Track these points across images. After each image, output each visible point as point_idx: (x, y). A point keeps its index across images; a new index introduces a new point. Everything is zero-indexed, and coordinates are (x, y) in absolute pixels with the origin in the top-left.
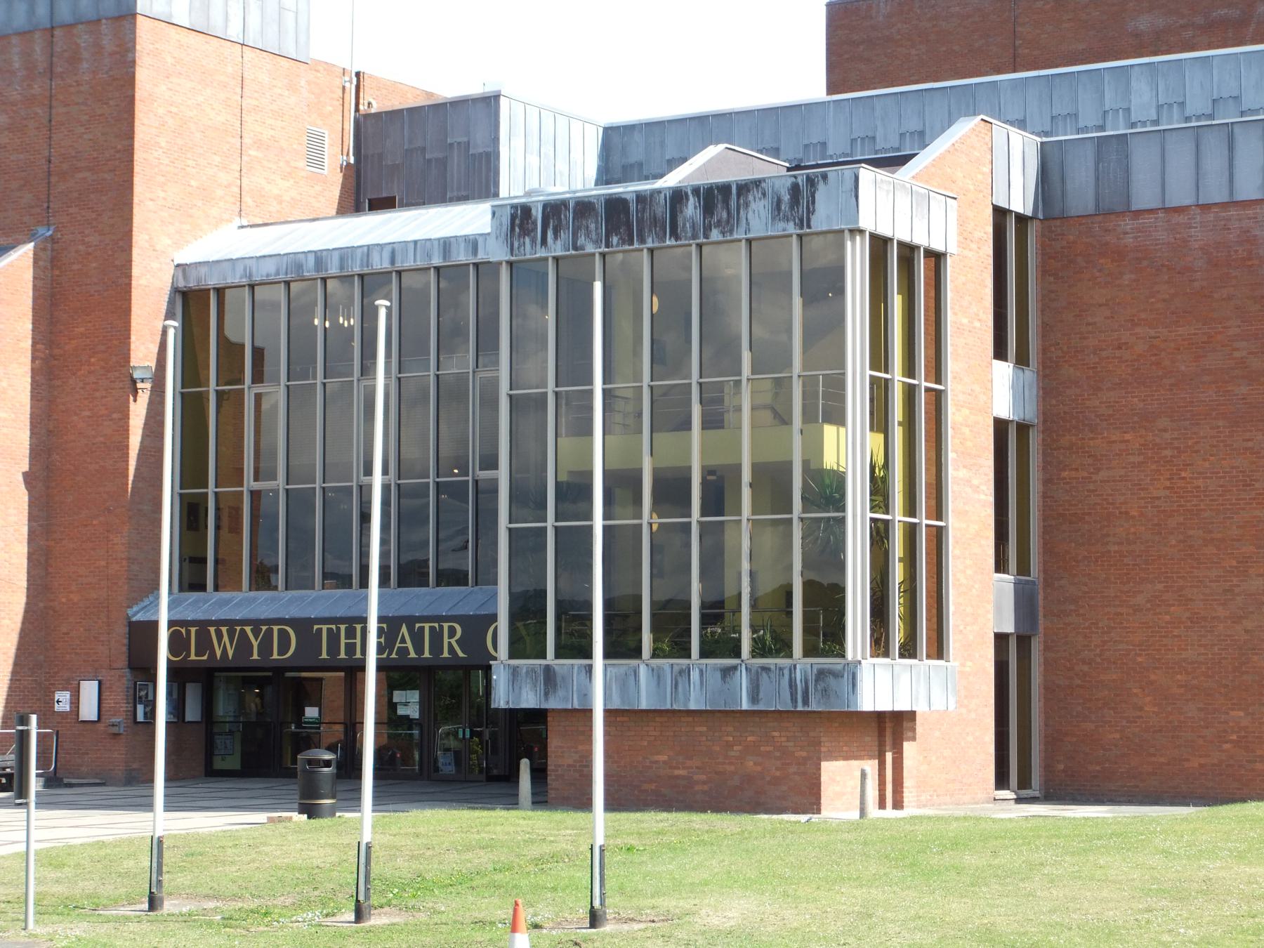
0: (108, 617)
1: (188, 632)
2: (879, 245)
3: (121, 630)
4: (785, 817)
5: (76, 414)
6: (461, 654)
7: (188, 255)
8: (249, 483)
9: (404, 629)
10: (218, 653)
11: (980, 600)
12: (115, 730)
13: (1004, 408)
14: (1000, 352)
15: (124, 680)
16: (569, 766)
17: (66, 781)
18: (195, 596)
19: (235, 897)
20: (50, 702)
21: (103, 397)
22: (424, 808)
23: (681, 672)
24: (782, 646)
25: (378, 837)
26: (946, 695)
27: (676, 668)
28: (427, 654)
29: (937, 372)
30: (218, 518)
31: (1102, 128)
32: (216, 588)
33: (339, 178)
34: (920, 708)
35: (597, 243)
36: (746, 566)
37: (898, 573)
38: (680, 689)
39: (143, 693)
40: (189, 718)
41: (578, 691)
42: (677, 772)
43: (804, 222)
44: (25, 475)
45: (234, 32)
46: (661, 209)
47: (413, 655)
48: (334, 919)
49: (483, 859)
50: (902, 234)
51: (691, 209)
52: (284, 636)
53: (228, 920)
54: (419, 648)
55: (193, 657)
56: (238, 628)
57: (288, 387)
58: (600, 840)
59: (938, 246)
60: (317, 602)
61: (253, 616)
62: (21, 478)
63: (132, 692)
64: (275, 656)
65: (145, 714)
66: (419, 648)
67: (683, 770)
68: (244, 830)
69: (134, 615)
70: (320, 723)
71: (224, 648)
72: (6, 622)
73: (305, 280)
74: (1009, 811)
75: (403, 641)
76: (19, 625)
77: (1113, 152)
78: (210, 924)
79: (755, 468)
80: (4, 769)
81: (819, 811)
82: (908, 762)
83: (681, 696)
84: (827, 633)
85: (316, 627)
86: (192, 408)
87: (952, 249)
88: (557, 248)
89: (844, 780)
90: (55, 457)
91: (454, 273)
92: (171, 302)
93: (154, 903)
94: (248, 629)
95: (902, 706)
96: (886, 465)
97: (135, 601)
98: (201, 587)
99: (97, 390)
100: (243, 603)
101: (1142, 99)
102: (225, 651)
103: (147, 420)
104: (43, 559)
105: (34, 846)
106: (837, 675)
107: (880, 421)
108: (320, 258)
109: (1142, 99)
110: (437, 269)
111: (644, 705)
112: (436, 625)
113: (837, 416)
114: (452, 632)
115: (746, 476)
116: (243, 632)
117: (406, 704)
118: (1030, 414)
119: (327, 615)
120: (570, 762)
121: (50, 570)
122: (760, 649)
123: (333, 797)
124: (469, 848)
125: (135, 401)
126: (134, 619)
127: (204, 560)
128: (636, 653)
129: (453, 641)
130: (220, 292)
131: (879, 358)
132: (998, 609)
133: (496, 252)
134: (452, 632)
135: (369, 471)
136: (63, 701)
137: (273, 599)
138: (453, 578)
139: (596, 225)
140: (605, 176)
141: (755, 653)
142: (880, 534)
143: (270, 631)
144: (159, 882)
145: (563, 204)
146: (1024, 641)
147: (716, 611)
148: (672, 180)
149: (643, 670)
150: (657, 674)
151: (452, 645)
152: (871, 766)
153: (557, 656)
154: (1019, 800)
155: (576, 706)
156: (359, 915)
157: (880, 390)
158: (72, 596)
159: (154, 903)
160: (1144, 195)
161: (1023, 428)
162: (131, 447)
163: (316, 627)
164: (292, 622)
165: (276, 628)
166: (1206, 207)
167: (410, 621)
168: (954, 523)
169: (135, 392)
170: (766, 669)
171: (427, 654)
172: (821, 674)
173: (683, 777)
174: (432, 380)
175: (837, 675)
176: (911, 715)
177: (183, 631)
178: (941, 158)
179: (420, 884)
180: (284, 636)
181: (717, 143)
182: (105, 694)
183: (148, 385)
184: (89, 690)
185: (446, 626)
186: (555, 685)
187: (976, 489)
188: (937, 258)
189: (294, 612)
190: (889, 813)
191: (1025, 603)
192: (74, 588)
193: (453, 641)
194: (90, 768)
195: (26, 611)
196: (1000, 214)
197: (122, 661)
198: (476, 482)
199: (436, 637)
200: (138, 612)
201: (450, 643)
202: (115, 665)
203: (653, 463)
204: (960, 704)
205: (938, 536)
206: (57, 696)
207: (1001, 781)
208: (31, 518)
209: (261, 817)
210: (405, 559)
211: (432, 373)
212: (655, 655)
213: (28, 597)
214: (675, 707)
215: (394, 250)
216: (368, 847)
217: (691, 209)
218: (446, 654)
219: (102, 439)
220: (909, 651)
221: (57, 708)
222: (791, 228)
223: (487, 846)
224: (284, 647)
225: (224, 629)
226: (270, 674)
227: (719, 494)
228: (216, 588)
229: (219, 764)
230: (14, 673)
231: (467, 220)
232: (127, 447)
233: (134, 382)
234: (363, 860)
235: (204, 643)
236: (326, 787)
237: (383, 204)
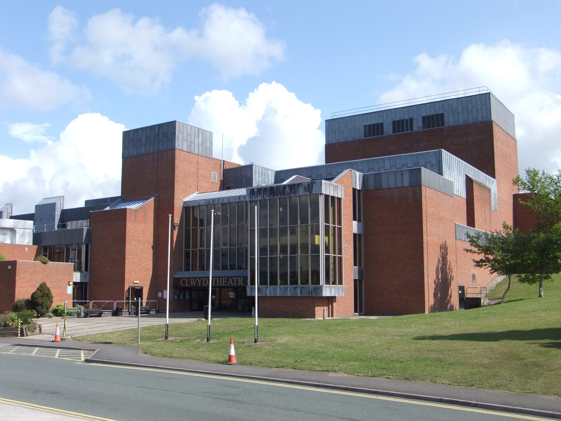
2: (327, 197)
4: (308, 319)
7: (187, 199)
8: (199, 248)
11: (350, 271)
13: (355, 230)
14: (354, 219)
19: (184, 337)
20: (157, 295)
24: (307, 282)
26: (342, 292)
29: (340, 223)
30: (192, 255)
31: (379, 171)
32: (192, 270)
33: (219, 183)
34: (337, 295)
35: (268, 197)
36: (299, 265)
37: (331, 266)
43: (311, 192)
45: (196, 152)
46: (281, 189)
49: (238, 328)
50: (332, 194)
51: (287, 189)
53: (181, 341)
54: (234, 284)
58: (209, 324)
59: (339, 197)
66: (234, 284)
67: (273, 309)
71: (193, 283)
73: (210, 204)
74: (357, 317)
77: (378, 176)
78: (176, 342)
79: (301, 244)
81: (314, 317)
82: (334, 307)
84: (316, 280)
86: (187, 232)
87: (343, 197)
88: (260, 198)
89: (320, 312)
91: (239, 202)
92: (183, 210)
93: (166, 338)
95: (333, 295)
96: (329, 243)
100: (186, 275)
101: (387, 164)
103: (172, 236)
105: (140, 327)
106: (318, 288)
107: (327, 233)
108: (213, 200)
109: (387, 164)
110: (238, 202)
111: (278, 295)
113: (318, 233)
114: (240, 280)
115: (299, 246)
118: (361, 232)
122: (302, 283)
124: (236, 326)
130: (193, 207)
131: (327, 220)
132: (355, 274)
133: (248, 199)
134: (240, 280)
135: (247, 244)
138: (240, 268)
139: (268, 193)
140: (276, 182)
141: (301, 284)
142: (327, 258)
145: (261, 188)
146: (360, 281)
147: (294, 275)
148: (285, 183)
150: (281, 288)
151: (240, 282)
152: (326, 308)
154: (359, 315)
156: (208, 341)
157: (327, 228)
160: (384, 185)
161: (360, 235)
166: (397, 188)
167: (232, 277)
168: (343, 256)
170: (303, 287)
172: (315, 288)
175: (318, 288)
176: (335, 297)
178: (341, 178)
181: (348, 168)
183: (8, 241)
187: (349, 248)
188: (339, 199)
190: (330, 318)
191: (360, 272)
196: (354, 190)
199: (237, 281)
204: (345, 294)
205: (340, 259)
207: (356, 311)
209: (196, 319)
212: (280, 285)
215: (229, 198)
217: (287, 189)
220: (334, 283)
222: (308, 193)
223: (240, 326)
227: (294, 249)
228: (192, 270)
229: (193, 308)
231: (242, 192)
235: (189, 282)
237: (229, 188)
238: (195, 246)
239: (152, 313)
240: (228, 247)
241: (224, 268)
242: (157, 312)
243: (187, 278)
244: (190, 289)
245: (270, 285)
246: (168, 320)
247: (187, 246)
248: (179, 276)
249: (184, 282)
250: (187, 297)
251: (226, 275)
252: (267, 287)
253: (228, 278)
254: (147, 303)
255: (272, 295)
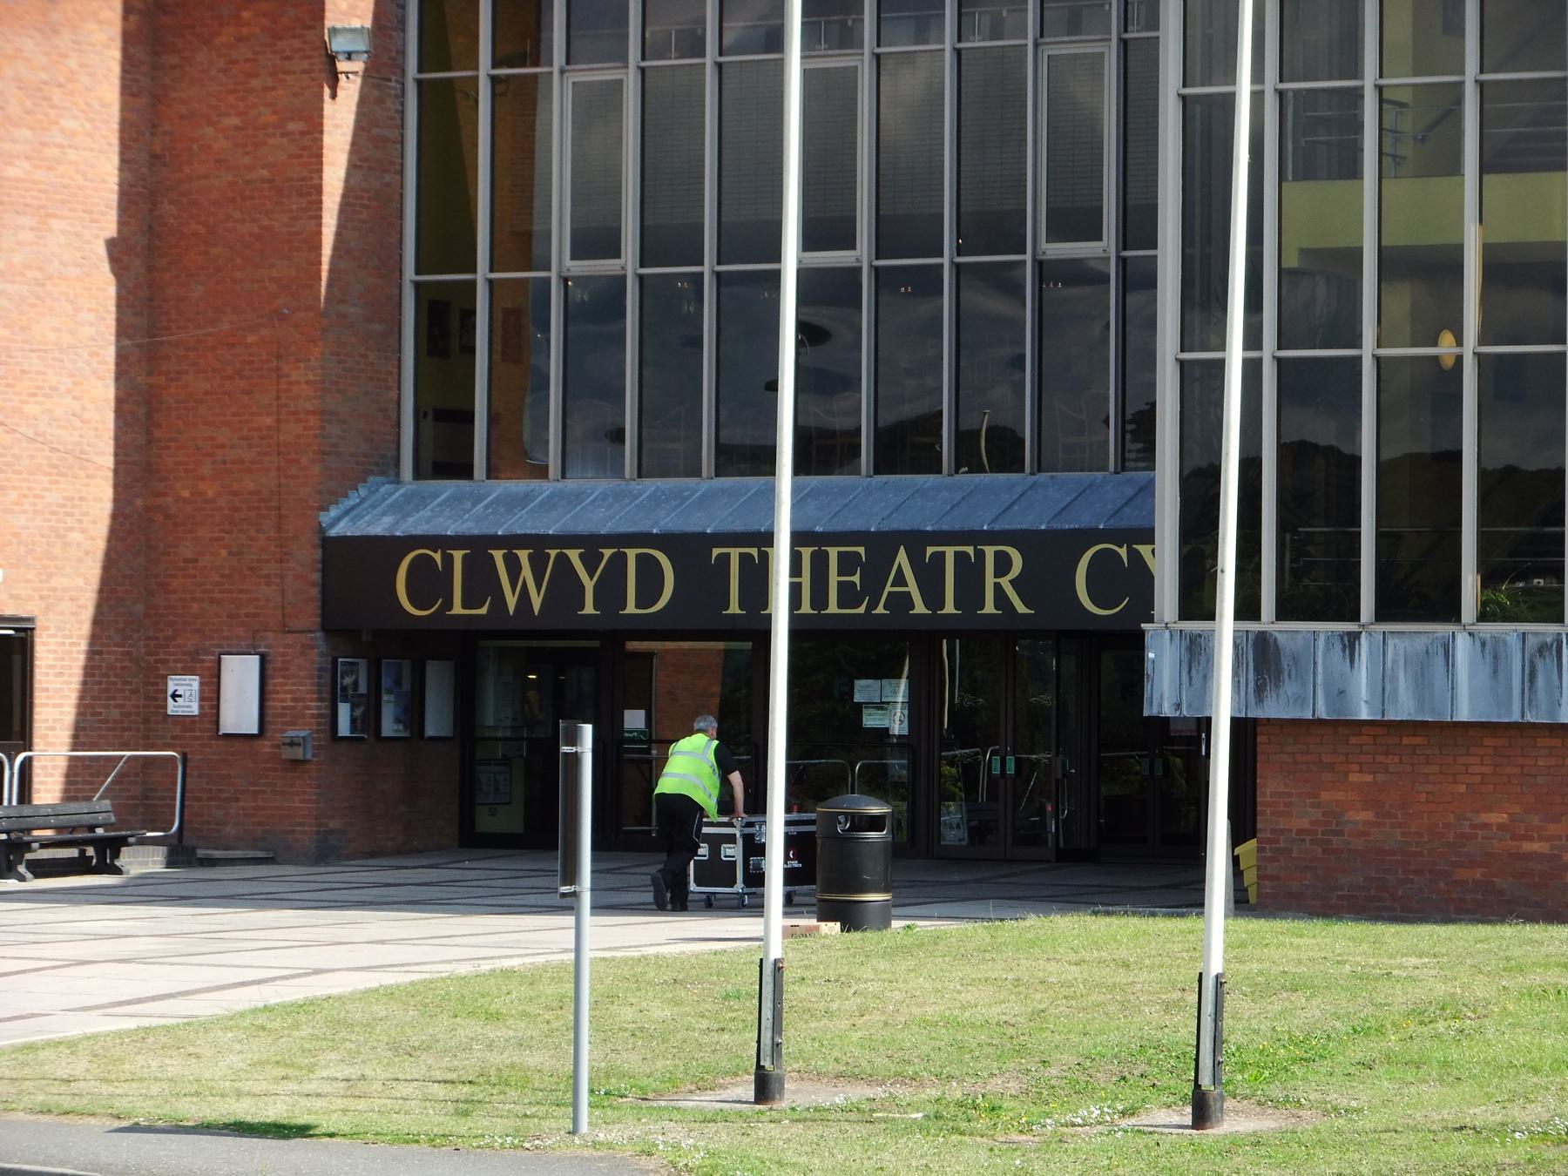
0: (279, 528)
1: (448, 560)
3: (307, 555)
5: (211, 123)
6: (1021, 608)
8: (562, 261)
9: (902, 557)
10: (512, 602)
12: (298, 753)
15: (314, 655)
16: (1300, 831)
17: (201, 853)
18: (449, 487)
20: (157, 696)
21: (266, 89)
22: (1047, 913)
23: (1542, 649)
25: (1235, 966)
27: (1532, 642)
28: (949, 608)
32: (492, 473)
38: (1541, 681)
39: (348, 681)
40: (431, 730)
41: (1327, 685)
42: (1527, 847)
44: (111, 245)
47: (920, 608)
48: (1133, 1121)
52: (649, 571)
54: (933, 596)
55: (458, 609)
56: (553, 553)
57: (643, 70)
58: (1216, 966)
60: (698, 502)
61: (582, 528)
62: (102, 251)
63: (327, 678)
64: (631, 608)
65: (353, 721)
66: (933, 596)
68: (749, 950)
69: (332, 525)
70: (650, 741)
71: (523, 590)
72: (76, 536)
75: (900, 580)
76: (101, 544)
80: (92, 828)
83: (1541, 694)
85: (716, 552)
86: (444, 112)
90: (166, 207)
94: (574, 555)
97: (334, 496)
98: (463, 470)
99: (256, 75)
102: (524, 597)
104: (142, 411)
111: (1464, 714)
112: (970, 550)
114: (1003, 564)
116: (563, 560)
117: (881, 706)
119: (738, 526)
120: (1305, 823)
121: (157, 433)
123: (886, 890)
125: (334, 96)
126: (333, 533)
127: (469, 417)
128: (1449, 610)
129: (1005, 582)
134: (1003, 564)
136: (184, 695)
137: (618, 496)
143: (619, 562)
144: (776, 1046)
149: (1462, 645)
150: (1493, 654)
153: (1283, 613)
155: (1322, 713)
158: (201, 485)
159: (765, 1088)
162: (327, 189)
163: (716, 552)
164: (666, 541)
165: (632, 554)
167: (915, 541)
169: (334, 79)
171: (949, 608)
173: (1541, 857)
174: (948, 56)
177: (437, 557)
179: (1308, 1052)
180: (649, 571)
182: (274, 682)
183: (358, 66)
184: (241, 677)
185: (990, 551)
186: (1279, 672)
189: (666, 521)
192: (206, 469)
193: (1005, 582)
194: (187, 822)
195: (116, 516)
197: (310, 617)
198: (1040, 265)
199: (970, 573)
200: (338, 519)
201: (998, 587)
202: (295, 624)
203: (1484, 235)
206: (173, 684)
208: (122, 330)
210: (887, 418)
211: (948, 47)
212: (1483, 617)
213: (116, 486)
214: (1529, 718)
216: (1219, 983)
218: (989, 608)
219: (265, 173)
221: (172, 708)
224: (649, 590)
225: (523, 555)
226: (596, 644)
228: (492, 473)
229: (486, 822)
230: (94, 638)
232: (319, 189)
233: (332, 59)
234: (1208, 1008)
235: (481, 582)
236: (873, 868)
238: (519, 242)
239: (142, 861)
240: (628, 261)
241: (905, 448)
242: (180, 854)
243: (458, 541)
244: (464, 648)
245: (1382, 615)
246: (773, 927)
247: (446, 238)
248: (380, 526)
249: (429, 582)
250: (437, 722)
251: (853, 523)
252: (1351, 642)
253: (882, 545)
254: (79, 777)
255: (1404, 708)
